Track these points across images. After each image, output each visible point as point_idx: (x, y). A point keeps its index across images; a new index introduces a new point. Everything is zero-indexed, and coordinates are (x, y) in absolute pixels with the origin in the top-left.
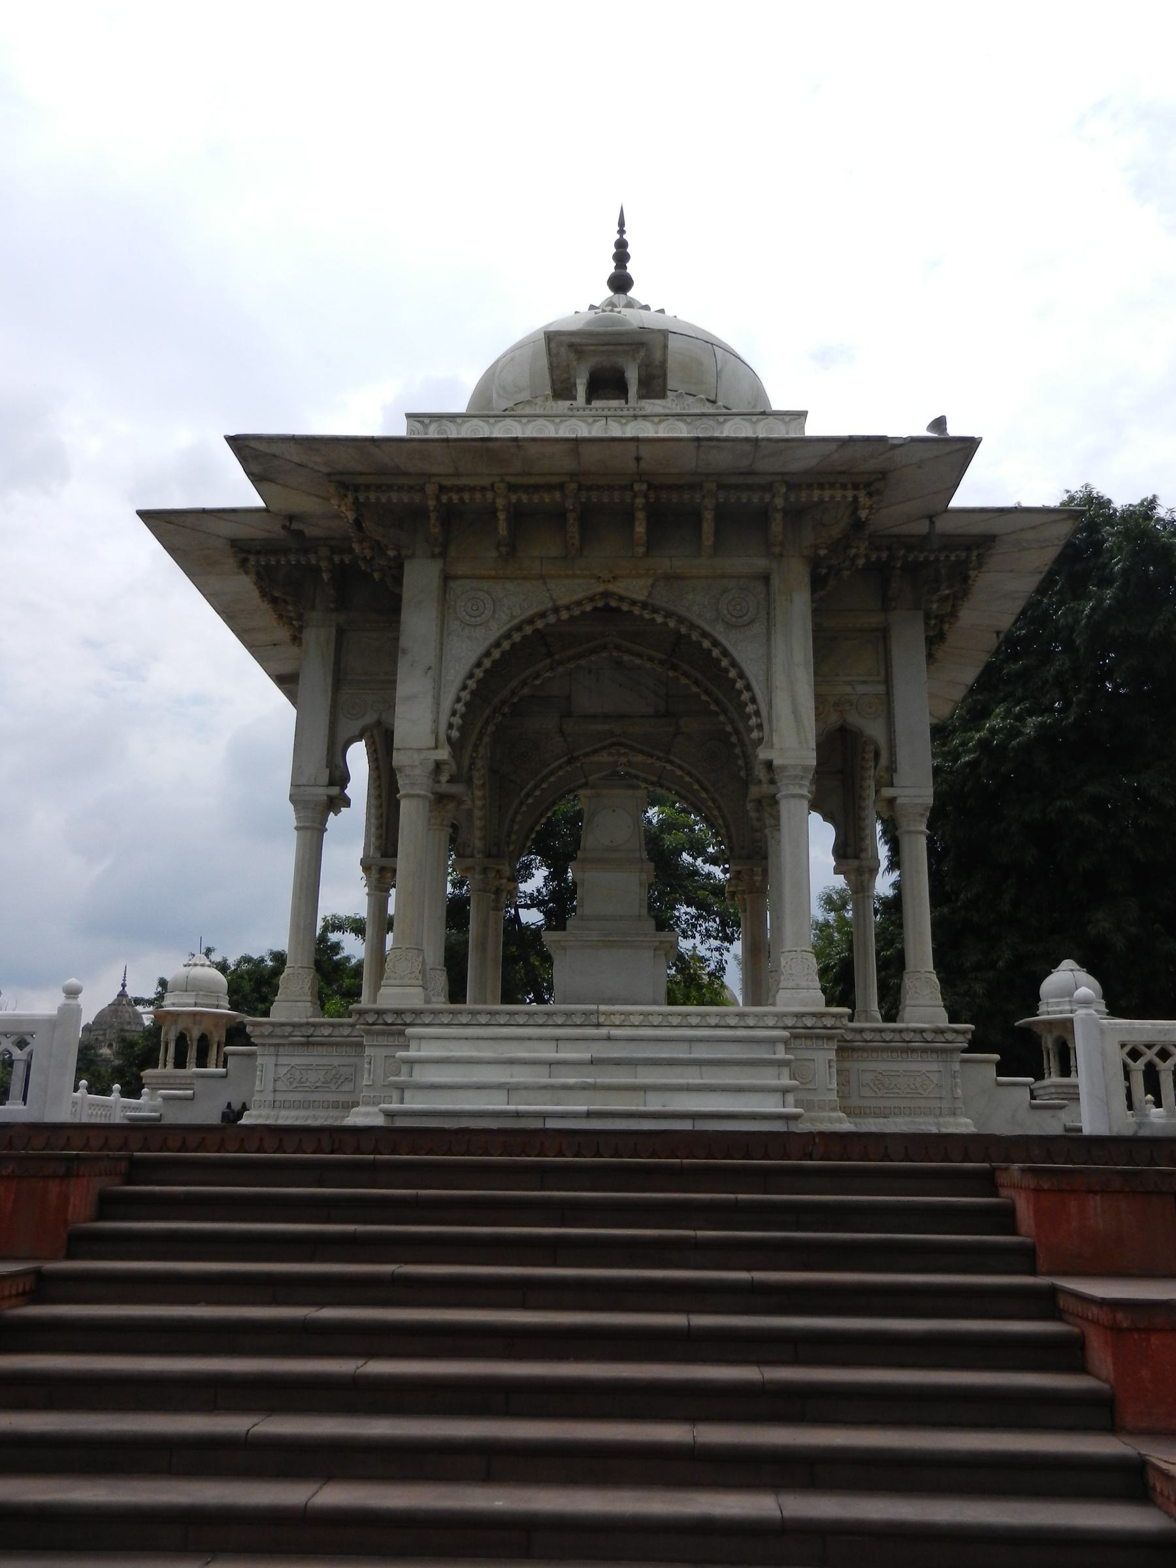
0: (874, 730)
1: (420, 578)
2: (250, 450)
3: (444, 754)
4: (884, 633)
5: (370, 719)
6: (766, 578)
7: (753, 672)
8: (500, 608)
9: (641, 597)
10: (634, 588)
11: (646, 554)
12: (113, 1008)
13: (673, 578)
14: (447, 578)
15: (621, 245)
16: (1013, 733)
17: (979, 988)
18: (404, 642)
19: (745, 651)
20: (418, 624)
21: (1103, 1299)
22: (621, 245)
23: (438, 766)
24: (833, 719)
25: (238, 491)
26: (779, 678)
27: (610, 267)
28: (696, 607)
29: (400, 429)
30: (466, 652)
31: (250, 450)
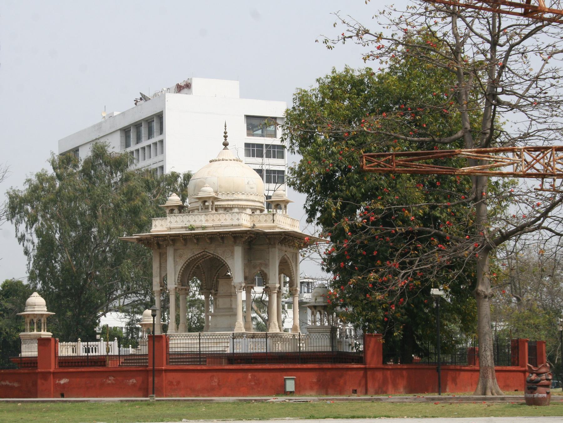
8: (188, 254)
15: (225, 133)
19: (229, 262)
22: (225, 133)
23: (176, 288)
27: (223, 140)
30: (181, 263)
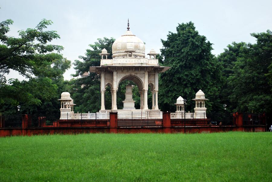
0: (153, 84)
1: (115, 73)
2: (75, 61)
3: (118, 89)
4: (155, 74)
5: (108, 83)
6: (144, 73)
7: (143, 82)
9: (134, 75)
10: (133, 74)
11: (134, 71)
12: (151, 105)
13: (136, 73)
14: (117, 73)
16: (176, 66)
17: (170, 99)
18: (114, 79)
19: (142, 80)
20: (115, 77)
21: (81, 132)
24: (150, 83)
25: (233, 46)
26: (145, 83)
27: (127, 27)
28: (138, 76)
29: (254, 41)
31: (75, 61)
